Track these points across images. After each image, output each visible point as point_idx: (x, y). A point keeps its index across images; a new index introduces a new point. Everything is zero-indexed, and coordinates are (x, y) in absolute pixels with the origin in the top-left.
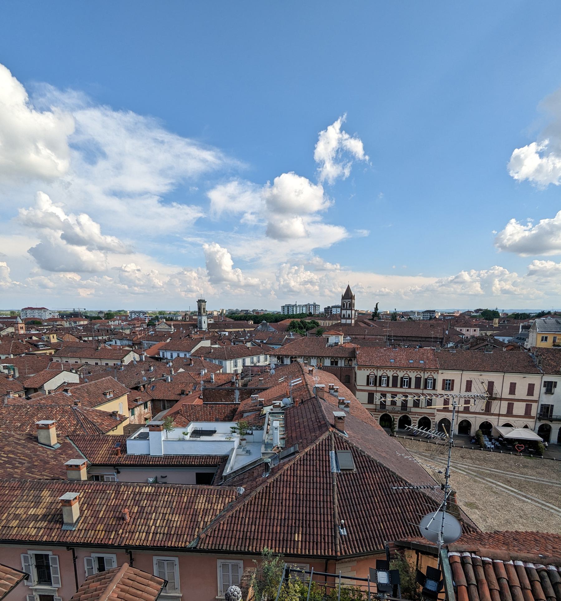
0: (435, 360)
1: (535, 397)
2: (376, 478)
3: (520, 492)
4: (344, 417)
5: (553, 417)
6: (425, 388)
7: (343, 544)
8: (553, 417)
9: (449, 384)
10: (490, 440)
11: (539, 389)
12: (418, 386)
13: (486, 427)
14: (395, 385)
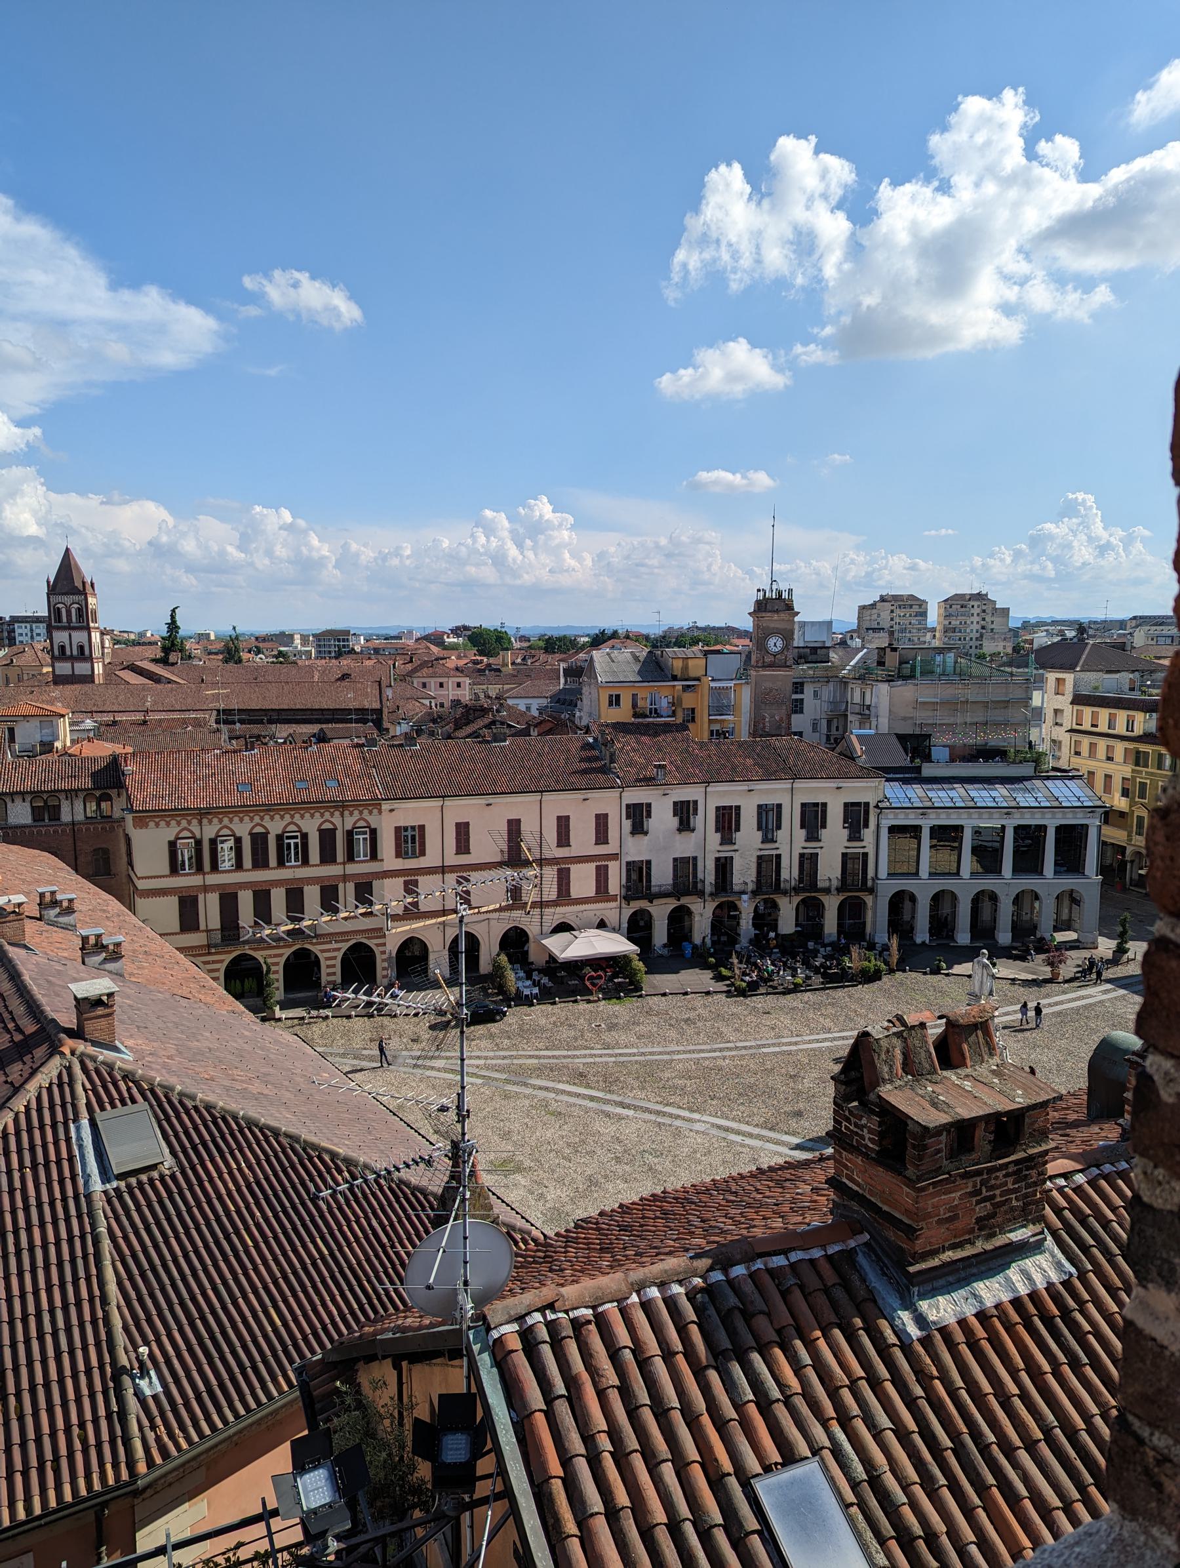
0: (370, 776)
1: (611, 848)
2: (240, 1169)
3: (608, 1096)
4: (110, 995)
5: (654, 890)
6: (351, 857)
7: (153, 1427)
8: (654, 890)
9: (413, 837)
11: (618, 825)
12: (328, 857)
13: (515, 941)
14: (260, 862)
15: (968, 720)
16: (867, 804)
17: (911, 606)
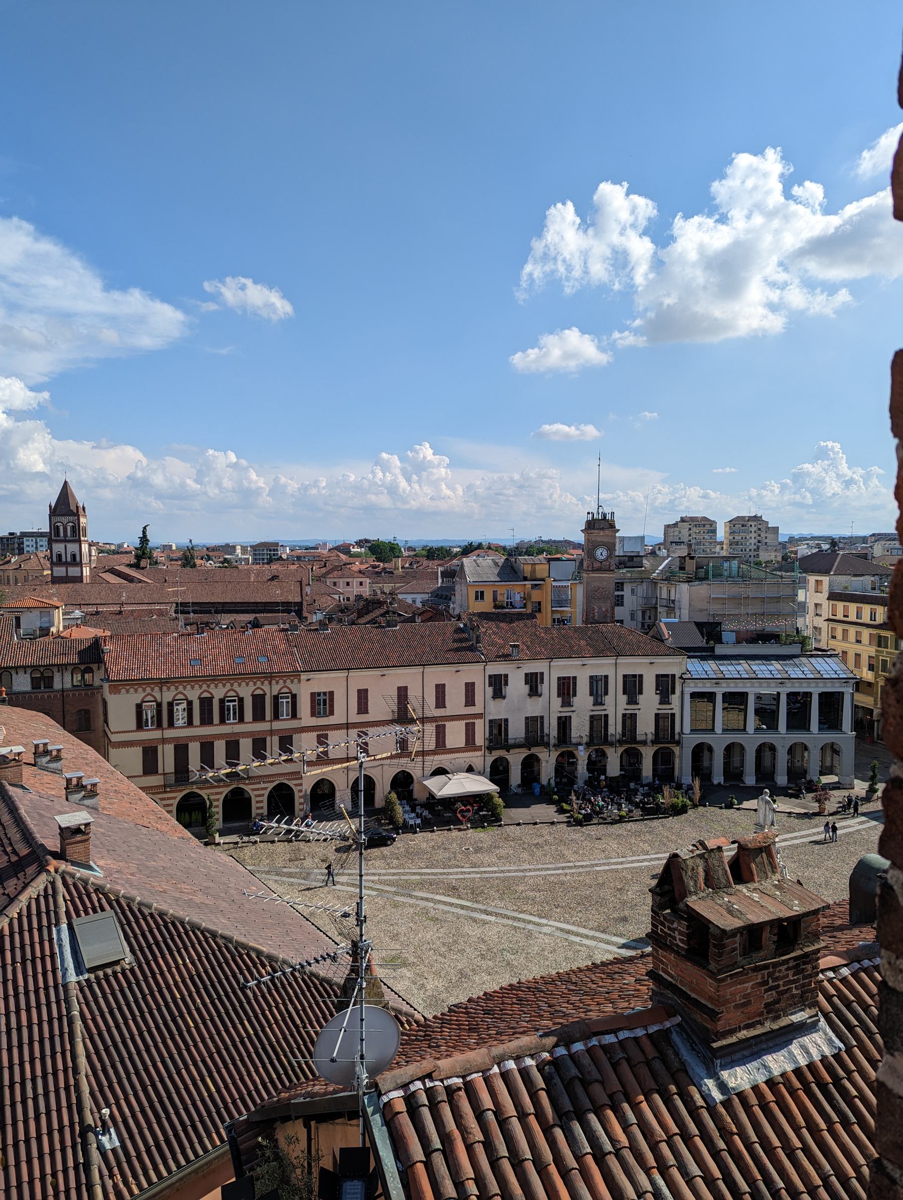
0: (292, 653)
2: (185, 965)
3: (475, 906)
5: (511, 742)
6: (276, 716)
7: (111, 1176)
8: (511, 742)
9: (325, 701)
10: (413, 810)
11: (483, 691)
12: (259, 716)
13: (403, 783)
15: (750, 612)
16: (673, 676)
17: (704, 525)
